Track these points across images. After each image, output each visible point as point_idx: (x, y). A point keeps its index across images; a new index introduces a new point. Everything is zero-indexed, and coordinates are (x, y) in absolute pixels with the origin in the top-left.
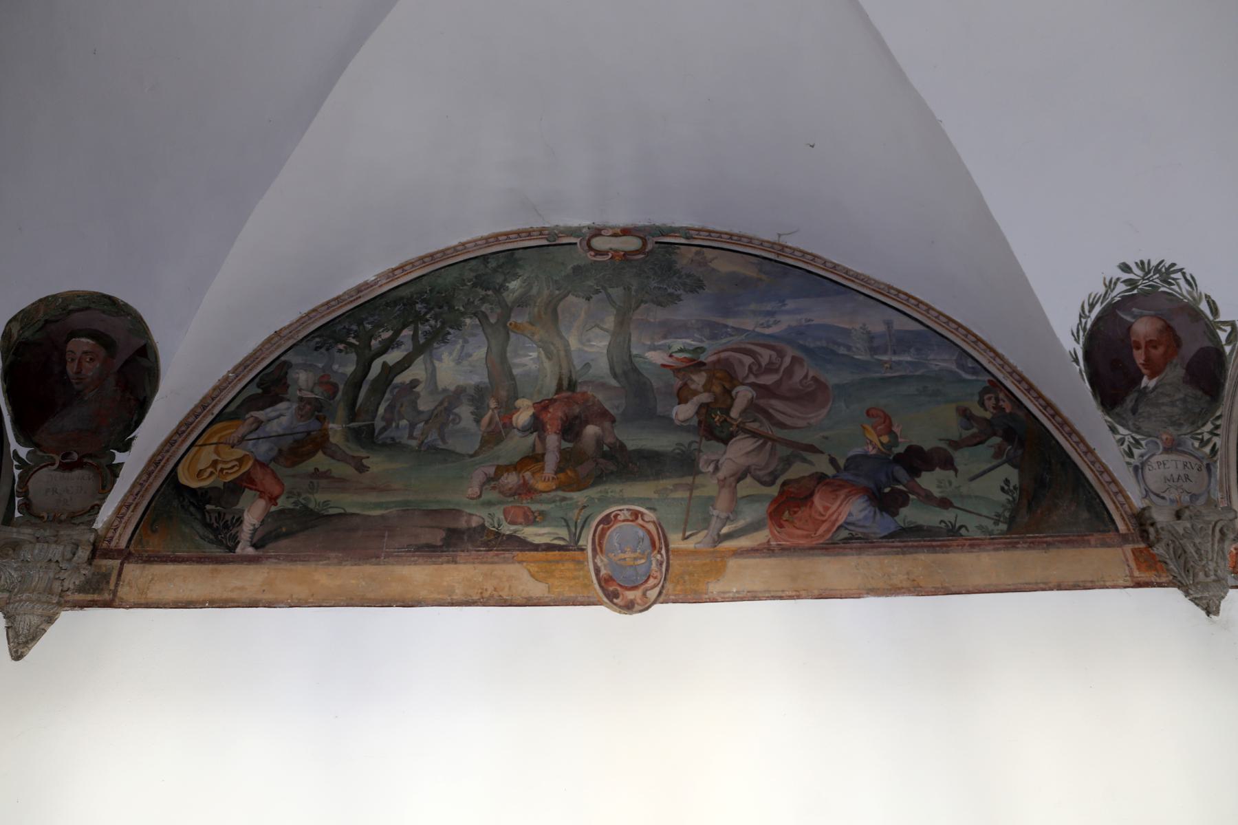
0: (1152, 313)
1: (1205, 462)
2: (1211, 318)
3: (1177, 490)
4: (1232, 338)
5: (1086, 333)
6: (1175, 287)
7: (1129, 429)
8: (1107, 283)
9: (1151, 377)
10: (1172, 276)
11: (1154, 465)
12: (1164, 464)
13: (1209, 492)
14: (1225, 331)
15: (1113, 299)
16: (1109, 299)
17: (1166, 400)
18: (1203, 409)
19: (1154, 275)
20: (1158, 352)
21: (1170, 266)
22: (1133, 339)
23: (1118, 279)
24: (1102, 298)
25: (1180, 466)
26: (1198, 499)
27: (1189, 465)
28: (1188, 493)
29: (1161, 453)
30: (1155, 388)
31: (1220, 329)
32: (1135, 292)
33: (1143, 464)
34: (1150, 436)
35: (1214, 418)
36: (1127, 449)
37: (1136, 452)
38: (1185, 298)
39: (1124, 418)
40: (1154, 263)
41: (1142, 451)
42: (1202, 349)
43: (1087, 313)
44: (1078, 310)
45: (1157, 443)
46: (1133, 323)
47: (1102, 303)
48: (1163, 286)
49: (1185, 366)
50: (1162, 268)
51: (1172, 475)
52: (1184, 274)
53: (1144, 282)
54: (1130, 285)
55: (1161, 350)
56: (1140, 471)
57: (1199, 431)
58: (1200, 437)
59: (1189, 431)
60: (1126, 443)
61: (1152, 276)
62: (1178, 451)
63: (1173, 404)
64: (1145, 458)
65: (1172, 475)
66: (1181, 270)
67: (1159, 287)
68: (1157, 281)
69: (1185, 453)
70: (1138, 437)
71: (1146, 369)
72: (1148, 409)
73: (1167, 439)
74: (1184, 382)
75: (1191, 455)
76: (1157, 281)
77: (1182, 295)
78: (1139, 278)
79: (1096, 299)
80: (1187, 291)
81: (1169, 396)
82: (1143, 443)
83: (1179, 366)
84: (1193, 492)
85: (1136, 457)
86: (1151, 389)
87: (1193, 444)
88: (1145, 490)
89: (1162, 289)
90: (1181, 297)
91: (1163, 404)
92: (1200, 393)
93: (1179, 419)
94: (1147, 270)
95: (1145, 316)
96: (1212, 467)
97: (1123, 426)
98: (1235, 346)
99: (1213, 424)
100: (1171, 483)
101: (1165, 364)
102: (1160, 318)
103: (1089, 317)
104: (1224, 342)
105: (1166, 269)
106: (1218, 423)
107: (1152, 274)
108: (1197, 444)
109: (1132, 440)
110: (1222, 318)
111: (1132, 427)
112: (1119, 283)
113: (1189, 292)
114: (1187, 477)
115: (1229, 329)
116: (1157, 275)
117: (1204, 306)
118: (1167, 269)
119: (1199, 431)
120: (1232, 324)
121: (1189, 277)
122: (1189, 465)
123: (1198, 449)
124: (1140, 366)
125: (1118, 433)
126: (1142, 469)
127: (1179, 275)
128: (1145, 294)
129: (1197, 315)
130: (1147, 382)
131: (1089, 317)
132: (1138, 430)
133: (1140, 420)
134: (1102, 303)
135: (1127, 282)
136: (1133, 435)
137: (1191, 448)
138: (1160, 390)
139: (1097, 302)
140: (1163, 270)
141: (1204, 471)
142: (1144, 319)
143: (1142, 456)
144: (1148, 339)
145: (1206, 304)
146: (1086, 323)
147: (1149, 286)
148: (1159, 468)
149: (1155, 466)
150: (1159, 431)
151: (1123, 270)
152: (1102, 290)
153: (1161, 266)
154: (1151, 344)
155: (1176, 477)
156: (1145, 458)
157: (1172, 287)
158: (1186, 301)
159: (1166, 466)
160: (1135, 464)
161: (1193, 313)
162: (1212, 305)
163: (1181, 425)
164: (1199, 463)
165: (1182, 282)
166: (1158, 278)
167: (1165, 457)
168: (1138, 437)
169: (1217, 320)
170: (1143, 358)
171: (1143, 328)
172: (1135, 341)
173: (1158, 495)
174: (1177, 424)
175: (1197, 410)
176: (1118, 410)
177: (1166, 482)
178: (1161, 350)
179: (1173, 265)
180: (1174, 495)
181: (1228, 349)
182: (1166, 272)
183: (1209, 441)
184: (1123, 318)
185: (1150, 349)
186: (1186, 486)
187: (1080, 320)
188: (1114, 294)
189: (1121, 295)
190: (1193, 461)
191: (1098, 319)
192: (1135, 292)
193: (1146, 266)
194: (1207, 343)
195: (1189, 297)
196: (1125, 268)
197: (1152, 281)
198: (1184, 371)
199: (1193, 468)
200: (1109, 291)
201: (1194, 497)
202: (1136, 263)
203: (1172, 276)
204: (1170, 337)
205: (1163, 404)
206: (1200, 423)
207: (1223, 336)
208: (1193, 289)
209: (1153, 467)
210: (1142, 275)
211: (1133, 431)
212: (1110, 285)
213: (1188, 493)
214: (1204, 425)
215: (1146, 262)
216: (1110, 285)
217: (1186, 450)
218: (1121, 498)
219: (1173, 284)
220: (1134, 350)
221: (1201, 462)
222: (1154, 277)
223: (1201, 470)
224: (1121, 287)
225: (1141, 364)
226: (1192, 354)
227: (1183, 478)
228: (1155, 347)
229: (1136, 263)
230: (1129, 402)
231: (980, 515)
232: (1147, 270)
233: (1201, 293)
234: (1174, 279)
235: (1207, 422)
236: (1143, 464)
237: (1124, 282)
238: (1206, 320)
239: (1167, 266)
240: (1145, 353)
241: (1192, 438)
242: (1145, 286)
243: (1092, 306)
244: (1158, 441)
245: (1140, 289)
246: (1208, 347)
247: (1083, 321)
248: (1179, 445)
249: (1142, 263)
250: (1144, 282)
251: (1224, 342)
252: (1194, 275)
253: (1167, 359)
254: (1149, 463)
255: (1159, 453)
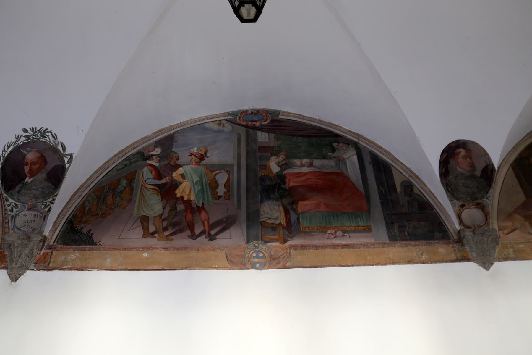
0: (36, 150)
1: (44, 215)
2: (62, 152)
3: (28, 226)
4: (70, 161)
5: (4, 158)
6: (47, 139)
7: (14, 200)
8: (17, 137)
9: (30, 178)
10: (46, 134)
11: (21, 216)
12: (26, 215)
13: (41, 228)
14: (67, 158)
15: (19, 144)
16: (17, 144)
17: (34, 188)
18: (50, 192)
19: (38, 134)
20: (35, 167)
21: (45, 130)
22: (25, 161)
23: (22, 135)
24: (14, 143)
25: (33, 216)
26: (35, 231)
27: (36, 216)
28: (32, 228)
29: (26, 211)
30: (31, 182)
31: (66, 157)
32: (29, 141)
33: (16, 215)
34: (23, 203)
35: (54, 195)
36: (11, 209)
37: (15, 210)
38: (52, 143)
39: (13, 195)
40: (38, 129)
41: (18, 209)
42: (56, 166)
43: (6, 150)
44: (2, 148)
45: (25, 206)
46: (27, 154)
47: (13, 146)
48: (42, 138)
49: (47, 173)
50: (41, 131)
51: (28, 220)
52: (52, 133)
53: (34, 136)
54: (27, 138)
55: (37, 166)
56: (14, 218)
57: (45, 201)
58: (45, 204)
59: (41, 201)
60: (11, 206)
61: (37, 134)
62: (33, 209)
63: (37, 189)
64: (18, 213)
65: (28, 220)
66: (50, 131)
67: (40, 139)
68: (39, 136)
69: (37, 210)
70: (17, 203)
71: (29, 174)
72: (26, 191)
73: (30, 204)
74: (44, 180)
75: (39, 211)
76: (39, 136)
77: (50, 142)
78: (31, 135)
79: (11, 144)
80: (53, 140)
81: (36, 186)
82: (19, 206)
83: (44, 173)
84: (34, 228)
85: (14, 212)
86: (29, 183)
87: (41, 207)
88: (14, 226)
89: (42, 140)
90: (50, 143)
91: (33, 189)
92: (50, 185)
93: (38, 196)
94: (35, 132)
95: (32, 151)
96: (46, 217)
97: (12, 198)
98: (70, 164)
99: (52, 198)
100: (26, 224)
101: (38, 172)
102: (39, 152)
103: (7, 151)
104: (66, 163)
105: (44, 131)
106: (55, 198)
107: (37, 133)
108: (43, 207)
109: (14, 205)
110: (67, 152)
111: (16, 199)
112: (22, 137)
113: (53, 141)
114: (34, 221)
115: (69, 157)
116: (40, 134)
117: (60, 147)
118: (44, 131)
119: (45, 201)
120: (71, 155)
121: (54, 135)
122: (36, 216)
123: (43, 209)
124: (26, 173)
125: (9, 201)
126: (15, 217)
127: (49, 134)
128: (33, 142)
129: (56, 151)
130: (28, 180)
131: (7, 151)
132: (18, 200)
133: (21, 196)
134: (13, 146)
135: (25, 136)
136: (16, 202)
137: (40, 209)
138: (33, 183)
139: (11, 145)
140: (42, 131)
141: (42, 218)
142: (32, 153)
143: (17, 212)
144: (32, 161)
145: (61, 146)
146: (5, 154)
147: (35, 138)
148: (23, 217)
149: (22, 216)
150: (28, 201)
151: (24, 132)
152: (14, 140)
153: (41, 130)
154: (33, 163)
155: (29, 221)
156: (18, 213)
157: (46, 139)
158: (52, 145)
159: (27, 216)
160: (13, 215)
161: (55, 150)
162: (63, 146)
163: (39, 198)
164: (41, 215)
165: (51, 137)
166: (39, 135)
167: (28, 212)
168: (17, 203)
169: (65, 153)
170: (28, 169)
171: (31, 156)
172: (26, 162)
173: (18, 229)
174: (36, 198)
175: (48, 192)
176: (11, 191)
177: (24, 223)
178: (37, 166)
179: (47, 129)
180: (25, 229)
181: (67, 166)
182: (44, 133)
183: (49, 205)
184: (22, 152)
185: (32, 165)
186: (32, 225)
187: (3, 153)
188: (19, 142)
189: (22, 142)
190: (39, 214)
191: (11, 152)
192: (29, 141)
193: (35, 130)
194: (59, 163)
195: (53, 143)
196: (25, 130)
197: (37, 136)
198: (46, 175)
199: (38, 217)
200: (17, 140)
201: (34, 230)
202: (30, 129)
203: (46, 134)
204: (43, 160)
205: (33, 189)
206: (47, 198)
207: (66, 160)
208: (55, 139)
209: (20, 216)
210: (32, 134)
211: (16, 201)
212: (18, 138)
213: (32, 228)
214: (48, 199)
215: (35, 128)
216: (18, 138)
217: (38, 210)
218: (7, 230)
219: (47, 138)
220: (25, 166)
221: (42, 215)
222: (38, 134)
223: (41, 218)
224: (23, 139)
225: (27, 172)
226: (51, 168)
227: (32, 222)
228: (35, 165)
229: (30, 129)
230: (17, 188)
231: (230, 234)
232: (35, 132)
233: (59, 141)
234: (47, 135)
235: (50, 197)
236: (16, 215)
237: (24, 136)
238: (60, 153)
239: (44, 130)
240: (30, 167)
241: (41, 204)
242: (34, 138)
243: (9, 147)
244: (26, 205)
245: (31, 139)
246: (58, 165)
247: (4, 153)
248: (35, 207)
249: (33, 128)
250: (34, 136)
251: (66, 163)
252: (56, 134)
253: (39, 170)
254: (19, 215)
255: (25, 210)
